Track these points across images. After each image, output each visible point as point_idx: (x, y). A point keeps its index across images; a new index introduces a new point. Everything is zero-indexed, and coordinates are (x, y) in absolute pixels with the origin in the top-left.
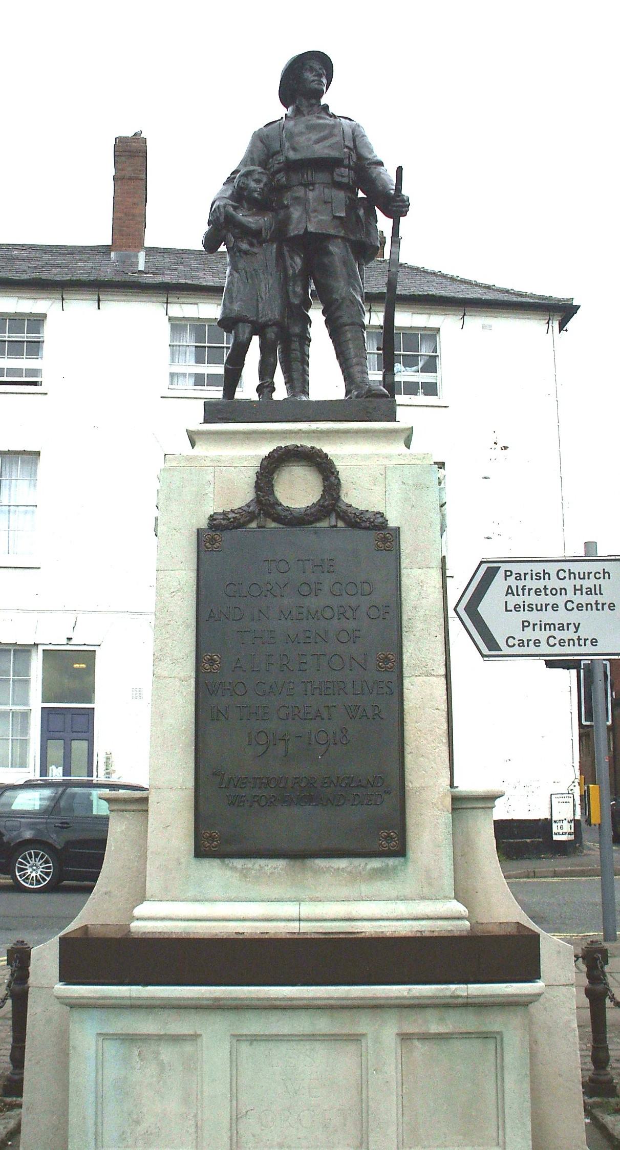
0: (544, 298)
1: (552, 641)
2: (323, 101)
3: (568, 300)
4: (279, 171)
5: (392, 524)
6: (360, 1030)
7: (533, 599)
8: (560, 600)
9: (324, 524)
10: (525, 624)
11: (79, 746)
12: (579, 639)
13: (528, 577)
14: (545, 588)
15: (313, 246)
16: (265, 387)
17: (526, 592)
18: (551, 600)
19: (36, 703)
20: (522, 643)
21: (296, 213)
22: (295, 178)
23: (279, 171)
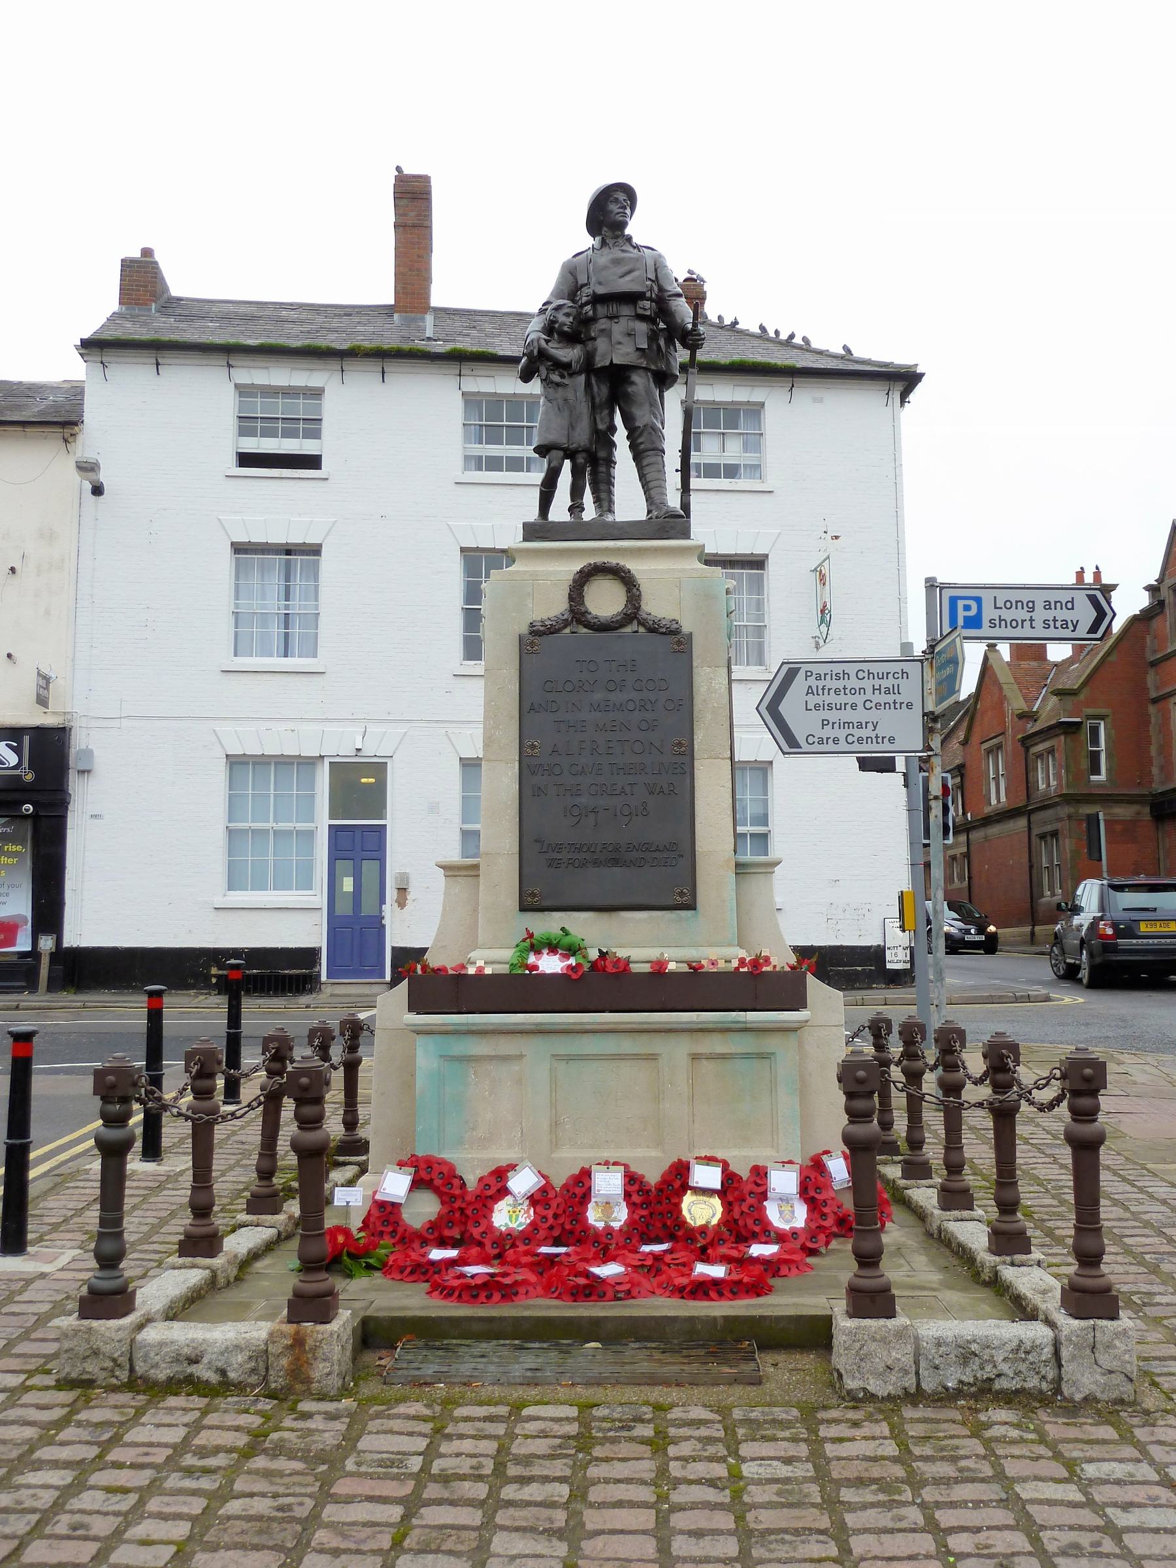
0: (886, 365)
1: (850, 739)
2: (627, 231)
3: (910, 367)
4: (586, 304)
5: (686, 629)
6: (657, 1050)
7: (832, 698)
8: (859, 699)
9: (628, 630)
10: (824, 723)
11: (369, 868)
12: (877, 737)
13: (828, 677)
14: (845, 689)
15: (617, 376)
16: (576, 508)
17: (826, 691)
18: (850, 699)
19: (323, 821)
20: (821, 741)
21: (601, 345)
22: (601, 310)
23: (586, 304)
